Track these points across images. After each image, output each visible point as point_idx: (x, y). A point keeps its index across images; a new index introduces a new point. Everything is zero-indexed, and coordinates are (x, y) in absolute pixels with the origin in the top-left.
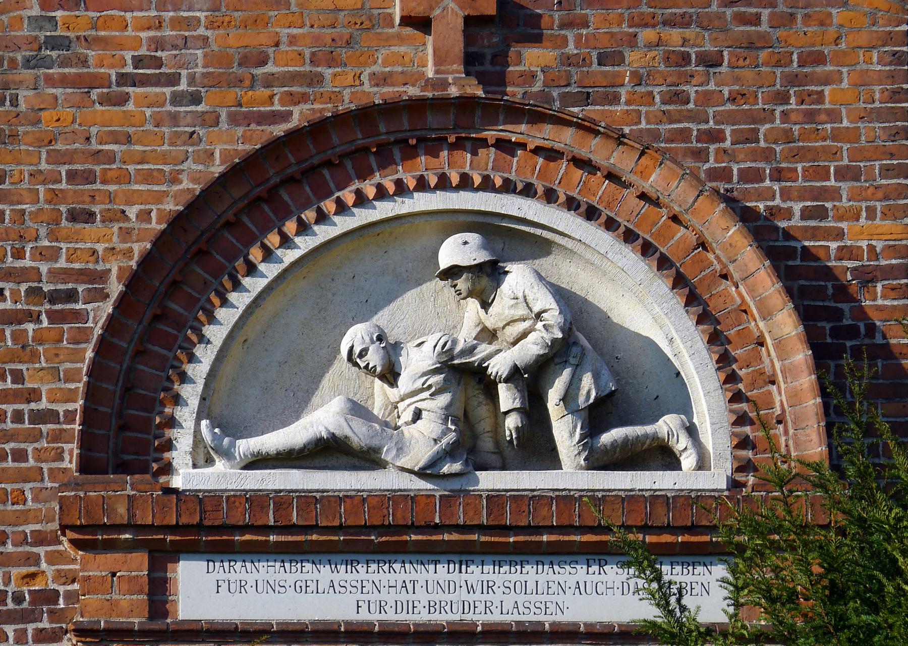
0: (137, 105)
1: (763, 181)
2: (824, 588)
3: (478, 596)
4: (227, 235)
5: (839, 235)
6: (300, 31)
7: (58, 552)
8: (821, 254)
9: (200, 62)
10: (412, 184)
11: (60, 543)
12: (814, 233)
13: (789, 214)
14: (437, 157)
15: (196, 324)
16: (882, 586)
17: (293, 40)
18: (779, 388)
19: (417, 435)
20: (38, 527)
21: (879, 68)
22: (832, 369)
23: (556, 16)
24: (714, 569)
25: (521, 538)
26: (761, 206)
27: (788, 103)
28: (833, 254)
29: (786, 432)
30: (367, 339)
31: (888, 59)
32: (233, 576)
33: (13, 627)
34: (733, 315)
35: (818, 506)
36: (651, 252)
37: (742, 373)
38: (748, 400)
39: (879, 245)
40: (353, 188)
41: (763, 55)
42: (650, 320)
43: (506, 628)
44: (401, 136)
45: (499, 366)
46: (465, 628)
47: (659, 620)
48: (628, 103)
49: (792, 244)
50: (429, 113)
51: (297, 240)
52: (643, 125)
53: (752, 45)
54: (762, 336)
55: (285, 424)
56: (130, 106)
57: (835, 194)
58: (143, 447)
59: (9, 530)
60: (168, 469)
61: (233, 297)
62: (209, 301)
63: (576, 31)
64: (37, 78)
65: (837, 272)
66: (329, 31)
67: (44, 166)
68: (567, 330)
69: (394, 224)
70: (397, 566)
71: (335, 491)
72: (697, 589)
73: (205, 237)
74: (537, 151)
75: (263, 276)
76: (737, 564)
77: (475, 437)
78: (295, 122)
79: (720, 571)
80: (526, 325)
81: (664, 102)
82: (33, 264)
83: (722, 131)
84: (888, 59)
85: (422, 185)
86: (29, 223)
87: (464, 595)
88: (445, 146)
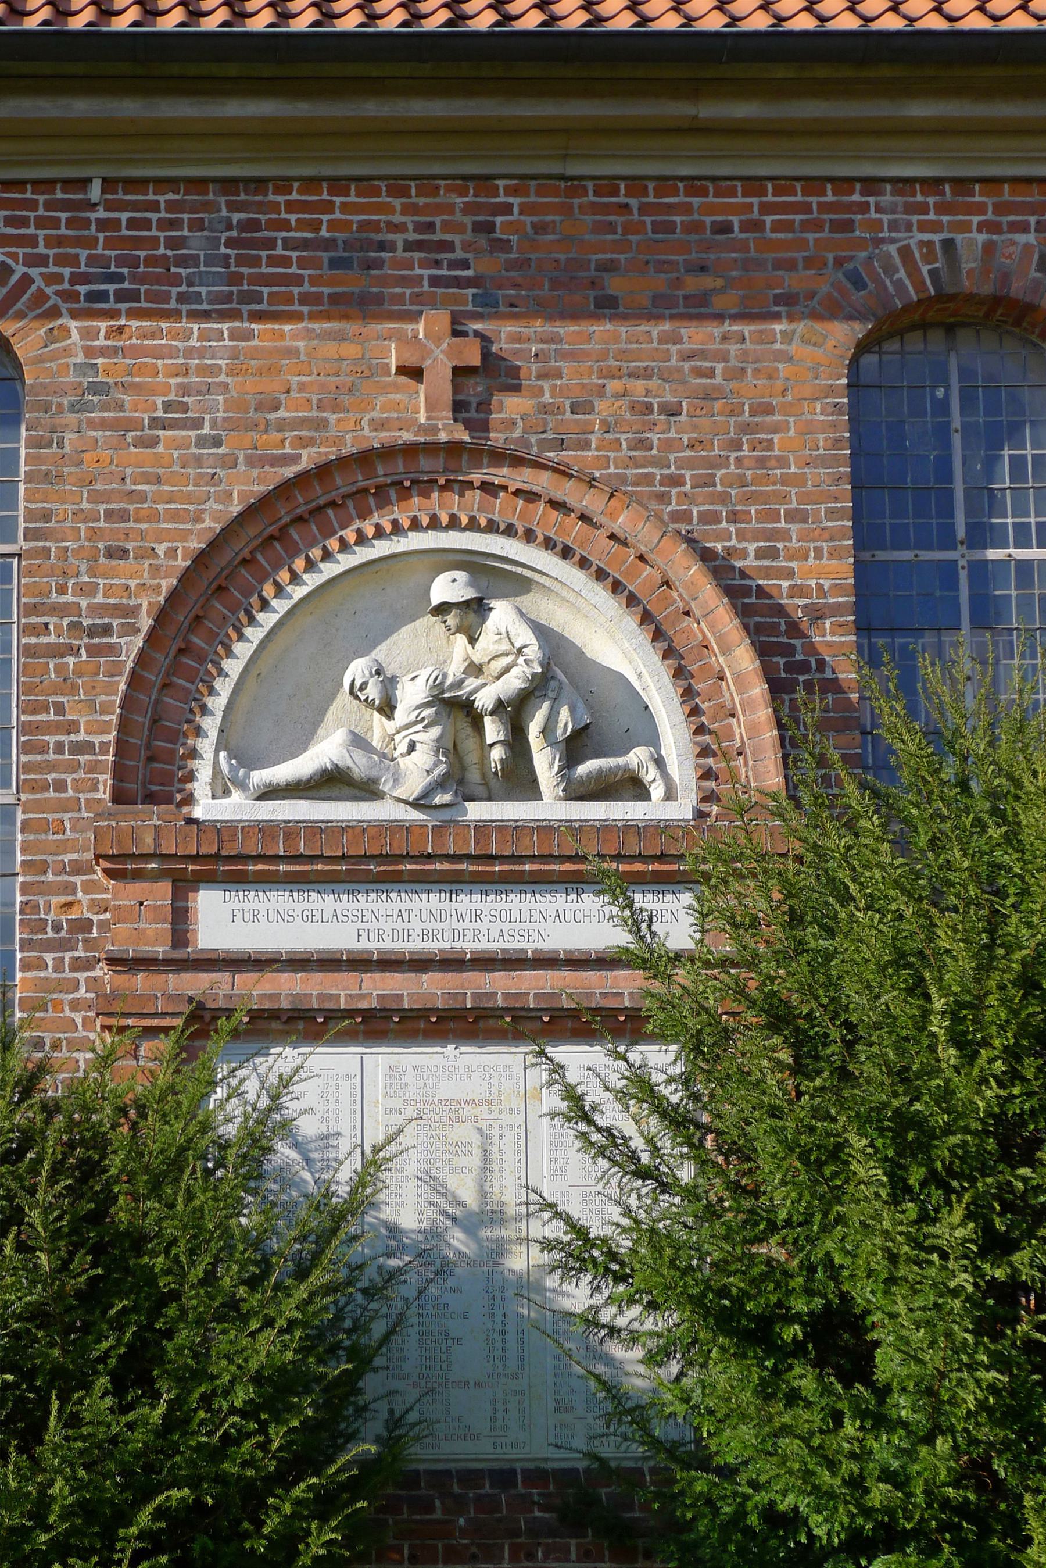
0: (166, 448)
1: (720, 522)
2: (784, 913)
3: (466, 924)
4: (243, 572)
5: (790, 574)
6: (308, 379)
7: (93, 881)
8: (774, 592)
9: (221, 408)
10: (406, 523)
11: (94, 872)
12: (768, 573)
13: (744, 554)
14: (429, 498)
15: (215, 658)
16: (836, 913)
17: (302, 388)
18: (739, 721)
19: (411, 766)
20: (75, 856)
21: (822, 418)
22: (787, 703)
23: (534, 367)
24: (681, 896)
25: (506, 867)
26: (719, 546)
27: (741, 450)
28: (785, 592)
29: (746, 764)
30: (367, 673)
31: (831, 409)
32: (247, 906)
33: (53, 955)
34: (695, 650)
35: (776, 834)
36: (620, 589)
37: (704, 706)
38: (710, 733)
39: (827, 584)
40: (355, 527)
41: (718, 405)
42: (620, 655)
43: (493, 956)
44: (396, 478)
45: (485, 700)
46: (455, 956)
47: (632, 946)
48: (597, 449)
49: (748, 582)
50: (421, 457)
51: (305, 577)
52: (612, 470)
53: (707, 396)
54: (722, 670)
55: (294, 756)
56: (160, 449)
57: (785, 536)
58: (167, 778)
59: (50, 859)
60: (189, 800)
61: (248, 631)
62: (227, 635)
63: (551, 382)
64: (80, 421)
65: (789, 609)
66: (333, 379)
67: (85, 505)
68: (546, 665)
69: (390, 562)
70: (394, 895)
71: (338, 821)
72: (668, 916)
73: (224, 573)
74: (517, 493)
75: (275, 611)
76: (702, 892)
77: (463, 769)
78: (304, 464)
79: (687, 898)
80: (509, 659)
81: (630, 449)
82: (75, 599)
83: (683, 476)
84: (831, 409)
85: (415, 525)
86: (71, 560)
87: (455, 924)
88: (436, 488)
